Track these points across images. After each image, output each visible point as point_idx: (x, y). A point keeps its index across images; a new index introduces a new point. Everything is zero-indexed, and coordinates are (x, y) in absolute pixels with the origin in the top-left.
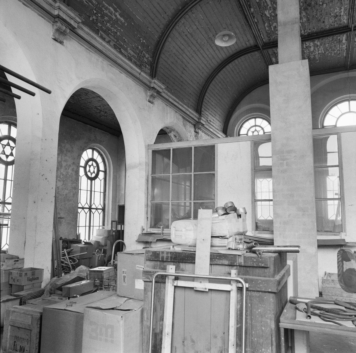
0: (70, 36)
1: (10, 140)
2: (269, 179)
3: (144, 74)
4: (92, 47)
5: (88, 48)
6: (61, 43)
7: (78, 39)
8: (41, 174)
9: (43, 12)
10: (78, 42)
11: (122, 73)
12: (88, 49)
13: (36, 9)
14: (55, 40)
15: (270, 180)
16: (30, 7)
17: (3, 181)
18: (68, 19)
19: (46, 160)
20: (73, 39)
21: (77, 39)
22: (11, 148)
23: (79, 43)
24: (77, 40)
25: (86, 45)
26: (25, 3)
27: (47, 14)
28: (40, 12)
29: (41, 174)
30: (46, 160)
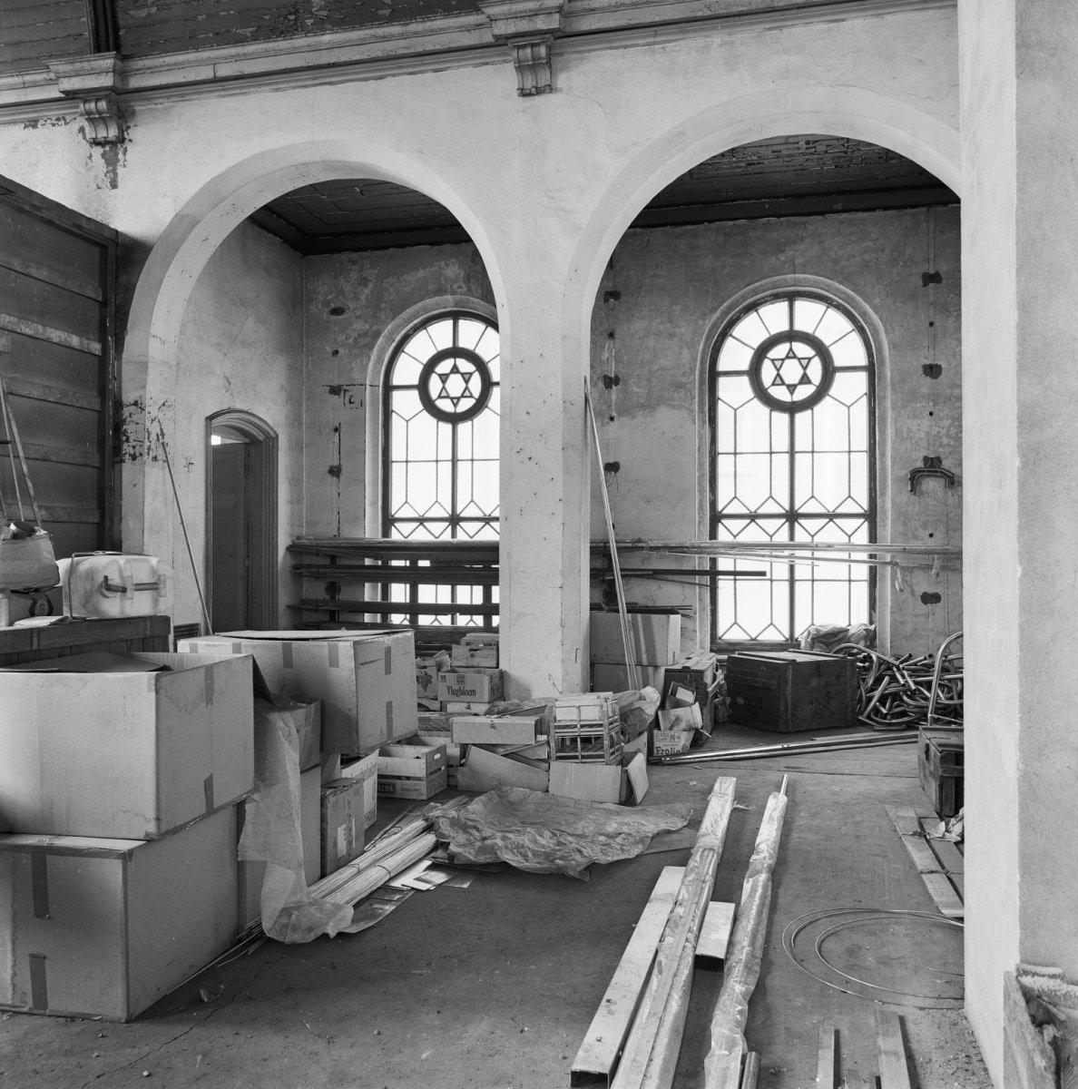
0: (577, 50)
1: (458, 357)
2: (735, 635)
3: (177, 57)
4: (659, 28)
5: (651, 40)
6: (550, 89)
7: (597, 43)
8: (514, 450)
9: (484, 52)
10: (611, 48)
11: (446, 69)
12: (654, 43)
13: (462, 60)
14: (524, 93)
15: (730, 632)
16: (448, 65)
17: (459, 458)
18: (524, 26)
19: (528, 413)
20: (589, 51)
21: (602, 42)
22: (464, 378)
23: (616, 48)
24: (605, 46)
25: (638, 38)
26: (378, 74)
27: (786, 12)
28: (473, 58)
29: (514, 450)
30: (528, 413)
